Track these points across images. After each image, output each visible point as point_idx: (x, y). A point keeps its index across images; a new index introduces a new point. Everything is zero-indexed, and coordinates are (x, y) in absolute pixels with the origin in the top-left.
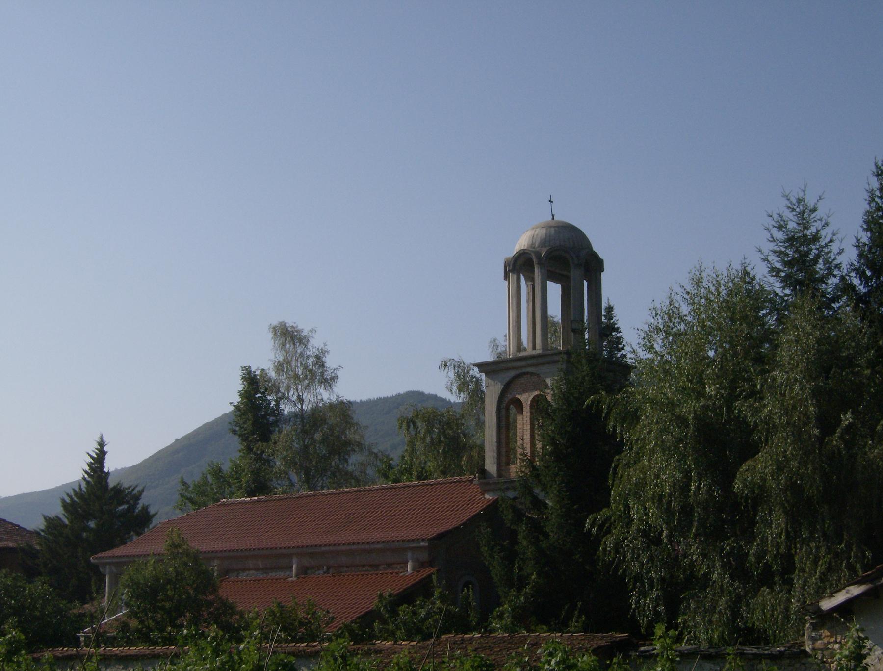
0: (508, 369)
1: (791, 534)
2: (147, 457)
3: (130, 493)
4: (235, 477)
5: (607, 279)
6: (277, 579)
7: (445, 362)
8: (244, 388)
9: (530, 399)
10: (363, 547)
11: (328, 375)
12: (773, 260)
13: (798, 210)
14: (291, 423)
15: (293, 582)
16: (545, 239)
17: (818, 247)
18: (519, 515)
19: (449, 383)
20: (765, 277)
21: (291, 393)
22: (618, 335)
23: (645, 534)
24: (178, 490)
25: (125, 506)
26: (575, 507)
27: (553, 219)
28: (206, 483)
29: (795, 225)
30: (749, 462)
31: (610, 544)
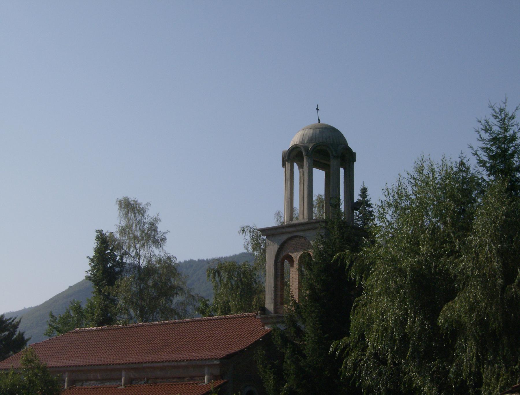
0: (282, 233)
1: (480, 358)
2: (48, 299)
3: (10, 323)
4: (90, 312)
5: (357, 167)
6: (110, 388)
7: (243, 228)
8: (97, 246)
9: (299, 256)
10: (172, 364)
11: (158, 237)
12: (481, 155)
13: (500, 117)
14: (131, 272)
15: (121, 389)
16: (312, 137)
17: (514, 145)
18: (286, 341)
19: (246, 244)
20: (476, 167)
21: (131, 250)
22: (371, 209)
23: (376, 356)
24: (47, 321)
25: (7, 333)
26: (326, 336)
27: (319, 122)
28: (68, 316)
29: (498, 129)
30: (450, 303)
31: (350, 362)
